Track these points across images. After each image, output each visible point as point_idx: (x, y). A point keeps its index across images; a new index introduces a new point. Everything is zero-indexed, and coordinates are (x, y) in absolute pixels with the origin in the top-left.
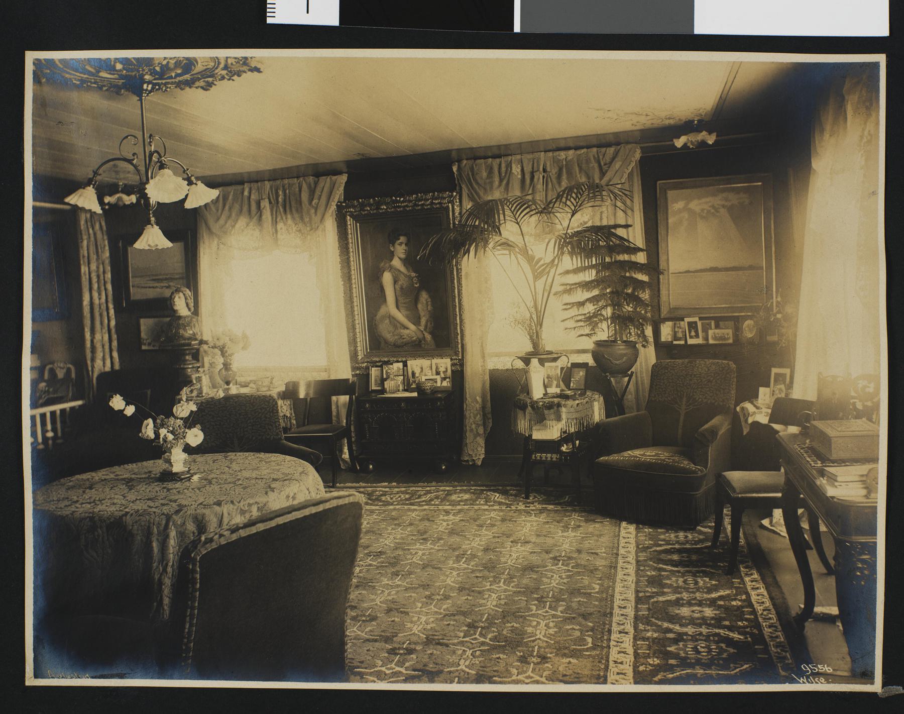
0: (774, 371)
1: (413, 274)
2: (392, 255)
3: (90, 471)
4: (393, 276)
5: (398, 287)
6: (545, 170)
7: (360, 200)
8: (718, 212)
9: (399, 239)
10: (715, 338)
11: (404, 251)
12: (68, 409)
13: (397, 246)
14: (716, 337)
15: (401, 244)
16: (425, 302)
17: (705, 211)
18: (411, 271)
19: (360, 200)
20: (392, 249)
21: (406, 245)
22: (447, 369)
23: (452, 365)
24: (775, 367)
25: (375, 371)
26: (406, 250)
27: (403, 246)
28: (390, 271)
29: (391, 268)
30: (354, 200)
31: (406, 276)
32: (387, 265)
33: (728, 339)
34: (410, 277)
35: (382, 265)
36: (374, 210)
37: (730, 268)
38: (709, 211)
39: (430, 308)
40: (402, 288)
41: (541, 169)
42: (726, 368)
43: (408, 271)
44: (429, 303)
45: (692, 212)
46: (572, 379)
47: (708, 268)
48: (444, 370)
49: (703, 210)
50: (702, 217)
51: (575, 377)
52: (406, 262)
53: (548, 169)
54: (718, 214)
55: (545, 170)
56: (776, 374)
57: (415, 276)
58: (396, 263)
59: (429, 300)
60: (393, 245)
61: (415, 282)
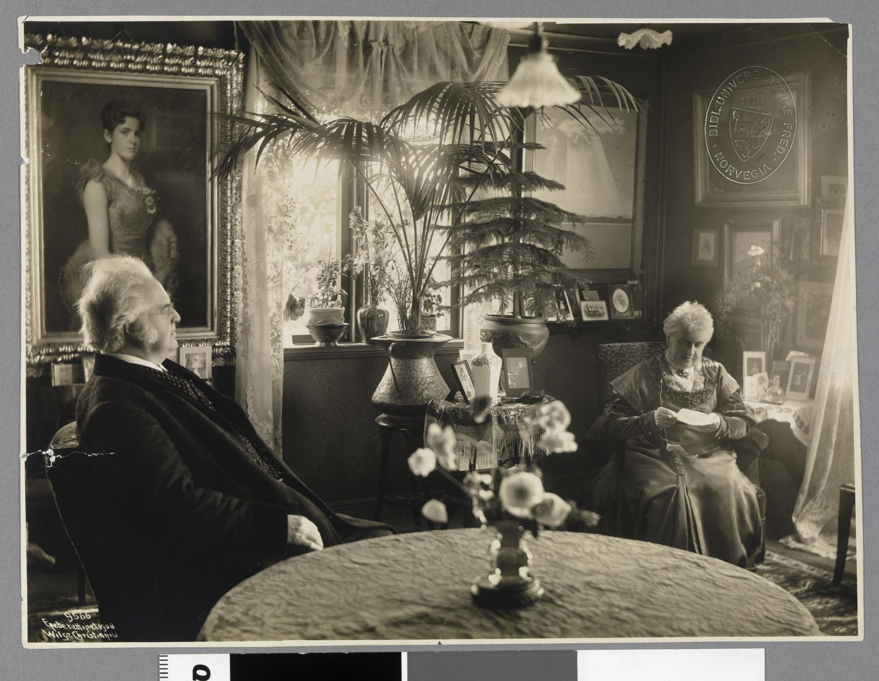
0: (747, 355)
1: (146, 191)
2: (107, 150)
4: (106, 189)
5: (114, 211)
7: (84, 40)
8: (590, 140)
9: (123, 122)
10: (589, 314)
12: (35, 548)
14: (589, 312)
15: (126, 131)
16: (165, 243)
17: (577, 137)
18: (142, 183)
19: (84, 40)
20: (108, 139)
21: (136, 134)
22: (204, 364)
23: (214, 356)
24: (749, 349)
25: (61, 370)
26: (135, 144)
27: (131, 136)
28: (100, 180)
29: (104, 176)
30: (36, 34)
31: (131, 191)
32: (96, 169)
33: (601, 315)
34: (141, 197)
38: (581, 137)
39: (174, 253)
40: (122, 215)
41: (381, 39)
45: (562, 135)
46: (509, 374)
48: (201, 366)
49: (574, 135)
53: (391, 41)
54: (590, 143)
55: (386, 41)
56: (749, 360)
57: (151, 195)
58: (116, 166)
59: (174, 239)
60: (111, 131)
61: (149, 204)
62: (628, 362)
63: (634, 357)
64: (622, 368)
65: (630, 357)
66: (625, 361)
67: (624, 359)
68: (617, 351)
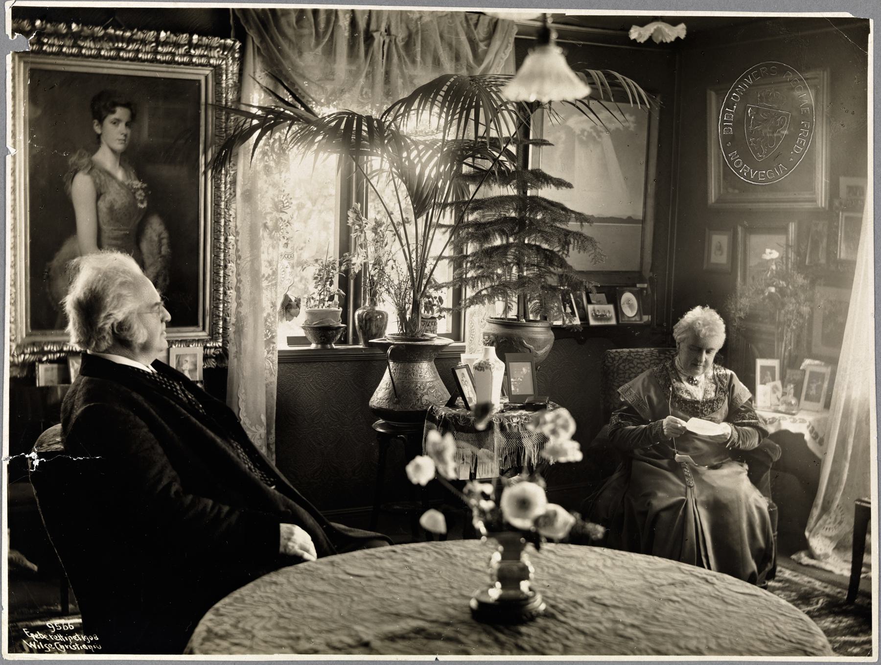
0: (760, 363)
1: (137, 184)
2: (98, 140)
3: (267, 571)
4: (95, 182)
5: (103, 205)
6: (388, 31)
8: (600, 136)
9: (114, 112)
11: (122, 137)
13: (107, 122)
14: (597, 316)
15: (116, 122)
16: (156, 239)
17: (586, 133)
18: (133, 176)
19: (74, 26)
20: (98, 130)
22: (195, 365)
23: (206, 358)
24: (763, 357)
25: (46, 370)
26: (126, 136)
27: (122, 127)
28: (89, 173)
29: (93, 168)
30: (24, 20)
31: (121, 184)
32: (85, 161)
33: (609, 319)
34: (132, 191)
35: (73, 159)
36: (148, 53)
37: (607, 218)
38: (590, 134)
39: (165, 250)
40: (111, 209)
41: (383, 29)
42: (617, 358)
43: (128, 176)
44: (165, 241)
45: (570, 131)
46: (512, 380)
47: (625, 218)
48: (192, 367)
49: (583, 131)
50: (582, 142)
51: (515, 376)
52: (126, 157)
54: (599, 140)
55: (388, 31)
56: (762, 367)
57: (142, 189)
58: (105, 158)
59: (165, 235)
60: (101, 121)
61: (140, 198)
62: (636, 368)
63: (643, 364)
64: (629, 374)
65: (638, 363)
66: (633, 368)
67: (631, 365)
68: (625, 358)
